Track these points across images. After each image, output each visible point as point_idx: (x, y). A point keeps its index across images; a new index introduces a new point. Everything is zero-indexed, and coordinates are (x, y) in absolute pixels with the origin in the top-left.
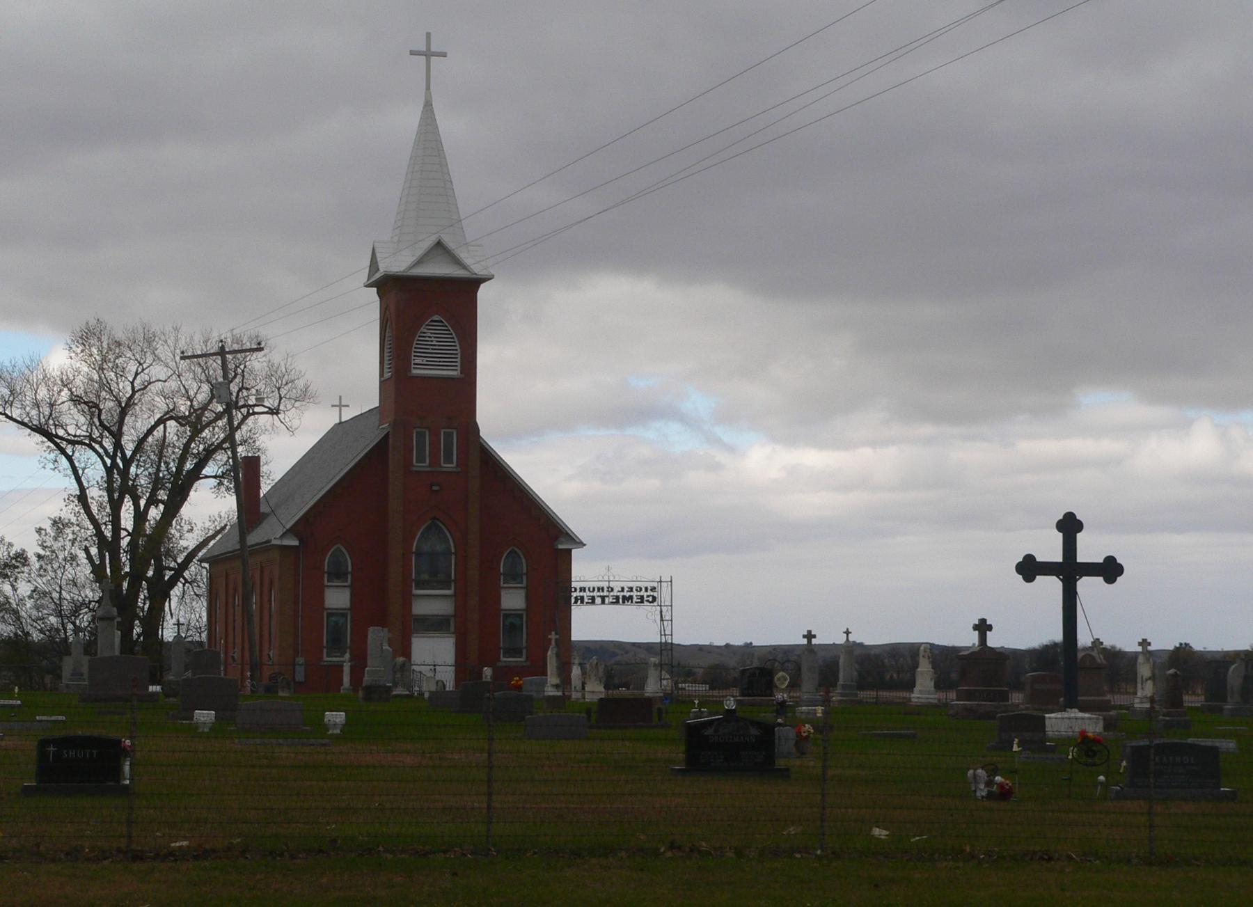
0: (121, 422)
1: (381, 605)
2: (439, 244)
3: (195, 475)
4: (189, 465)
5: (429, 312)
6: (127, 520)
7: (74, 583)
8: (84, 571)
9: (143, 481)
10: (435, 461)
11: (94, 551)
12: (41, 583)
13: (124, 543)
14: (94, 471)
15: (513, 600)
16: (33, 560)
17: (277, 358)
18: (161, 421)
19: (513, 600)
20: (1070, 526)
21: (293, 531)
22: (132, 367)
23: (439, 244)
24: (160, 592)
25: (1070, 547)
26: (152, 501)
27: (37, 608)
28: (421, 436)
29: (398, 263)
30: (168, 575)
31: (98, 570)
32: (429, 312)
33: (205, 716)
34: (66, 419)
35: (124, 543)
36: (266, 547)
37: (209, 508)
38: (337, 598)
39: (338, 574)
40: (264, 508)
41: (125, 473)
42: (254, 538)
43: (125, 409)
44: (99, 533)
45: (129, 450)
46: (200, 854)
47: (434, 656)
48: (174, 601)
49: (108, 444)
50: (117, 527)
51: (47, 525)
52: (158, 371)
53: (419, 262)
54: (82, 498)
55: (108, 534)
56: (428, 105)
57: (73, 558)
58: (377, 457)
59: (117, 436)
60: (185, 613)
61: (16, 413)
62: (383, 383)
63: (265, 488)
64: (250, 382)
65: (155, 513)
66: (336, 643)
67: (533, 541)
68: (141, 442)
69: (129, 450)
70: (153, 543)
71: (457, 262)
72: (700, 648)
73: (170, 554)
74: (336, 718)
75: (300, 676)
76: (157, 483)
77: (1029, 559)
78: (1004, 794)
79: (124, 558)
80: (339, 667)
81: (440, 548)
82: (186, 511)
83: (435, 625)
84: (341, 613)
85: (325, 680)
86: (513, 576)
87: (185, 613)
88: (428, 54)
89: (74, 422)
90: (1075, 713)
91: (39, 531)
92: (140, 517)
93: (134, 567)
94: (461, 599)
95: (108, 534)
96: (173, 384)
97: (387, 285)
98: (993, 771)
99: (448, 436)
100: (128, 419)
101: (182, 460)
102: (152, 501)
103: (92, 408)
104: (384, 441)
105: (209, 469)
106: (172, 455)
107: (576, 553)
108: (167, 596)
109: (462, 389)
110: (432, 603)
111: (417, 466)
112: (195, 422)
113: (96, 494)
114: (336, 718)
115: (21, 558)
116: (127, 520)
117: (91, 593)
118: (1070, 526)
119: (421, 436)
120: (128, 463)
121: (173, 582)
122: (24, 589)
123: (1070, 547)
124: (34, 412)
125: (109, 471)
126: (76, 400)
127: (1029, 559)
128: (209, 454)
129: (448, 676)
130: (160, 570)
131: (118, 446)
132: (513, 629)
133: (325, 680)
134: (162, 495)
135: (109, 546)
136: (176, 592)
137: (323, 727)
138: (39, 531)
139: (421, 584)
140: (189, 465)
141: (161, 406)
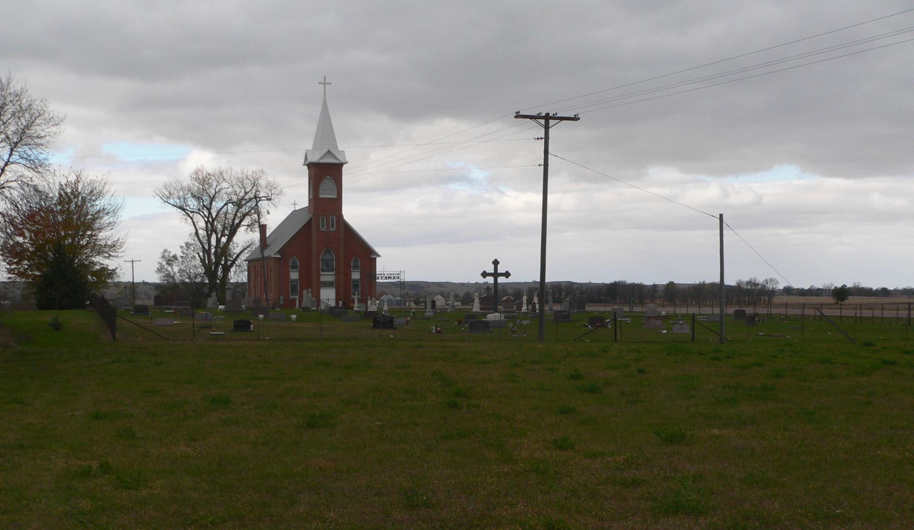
0: (211, 204)
1: (310, 282)
2: (329, 152)
3: (239, 225)
4: (237, 221)
5: (325, 174)
6: (213, 242)
7: (195, 266)
8: (198, 262)
9: (219, 226)
10: (328, 228)
11: (201, 254)
12: (183, 267)
13: (213, 251)
14: (201, 224)
15: (356, 275)
16: (180, 260)
17: (270, 179)
18: (226, 204)
19: (356, 275)
20: (496, 263)
21: (279, 252)
22: (215, 184)
23: (329, 152)
24: (226, 269)
25: (496, 269)
26: (222, 235)
27: (181, 276)
28: (323, 221)
29: (315, 158)
30: (229, 263)
31: (202, 261)
32: (325, 174)
33: (261, 316)
34: (189, 203)
35: (213, 251)
36: (269, 258)
37: (245, 238)
38: (294, 275)
39: (294, 267)
40: (268, 242)
41: (212, 224)
42: (267, 253)
43: (212, 199)
44: (203, 247)
45: (214, 214)
46: (270, 340)
47: (328, 296)
48: (232, 273)
49: (206, 213)
50: (210, 245)
51: (184, 245)
52: (225, 185)
53: (322, 158)
54: (197, 233)
55: (207, 248)
56: (325, 101)
57: (194, 257)
58: (307, 227)
59: (209, 210)
60: (238, 275)
61: (171, 201)
62: (310, 200)
63: (268, 234)
64: (259, 189)
65: (224, 240)
66: (294, 290)
67: (365, 255)
68: (218, 213)
69: (214, 214)
70: (223, 250)
71: (335, 158)
72: (463, 284)
73: (230, 256)
74: (294, 317)
75: (282, 303)
76: (224, 228)
77: (484, 272)
78: (439, 332)
79: (213, 257)
80: (295, 300)
81: (330, 258)
82: (235, 239)
83: (328, 285)
84: (295, 281)
85: (290, 304)
86: (356, 267)
87: (238, 275)
88: (325, 83)
89: (193, 204)
90: (497, 314)
91: (181, 247)
92: (218, 241)
93: (217, 258)
94: (337, 275)
95: (207, 248)
96: (230, 190)
97: (312, 166)
98: (437, 327)
99: (332, 219)
100: (214, 203)
101: (234, 220)
102: (222, 235)
103: (199, 198)
104: (310, 221)
105: (245, 222)
106: (230, 216)
107: (378, 259)
108: (229, 271)
109: (337, 202)
110: (327, 277)
111: (322, 229)
112: (239, 204)
113: (202, 233)
114: (294, 317)
115: (175, 257)
116: (213, 242)
117: (201, 270)
118: (496, 263)
119: (323, 221)
120: (213, 220)
121: (231, 265)
122: (176, 269)
123: (496, 269)
124: (178, 201)
125: (206, 223)
126: (194, 196)
127: (484, 272)
128: (244, 216)
129: (332, 303)
130: (226, 261)
131: (210, 213)
132: (356, 286)
133: (290, 304)
134: (227, 232)
135: (207, 252)
136: (233, 269)
137: (290, 319)
138: (181, 247)
139: (323, 271)
140: (237, 221)
141: (226, 198)
